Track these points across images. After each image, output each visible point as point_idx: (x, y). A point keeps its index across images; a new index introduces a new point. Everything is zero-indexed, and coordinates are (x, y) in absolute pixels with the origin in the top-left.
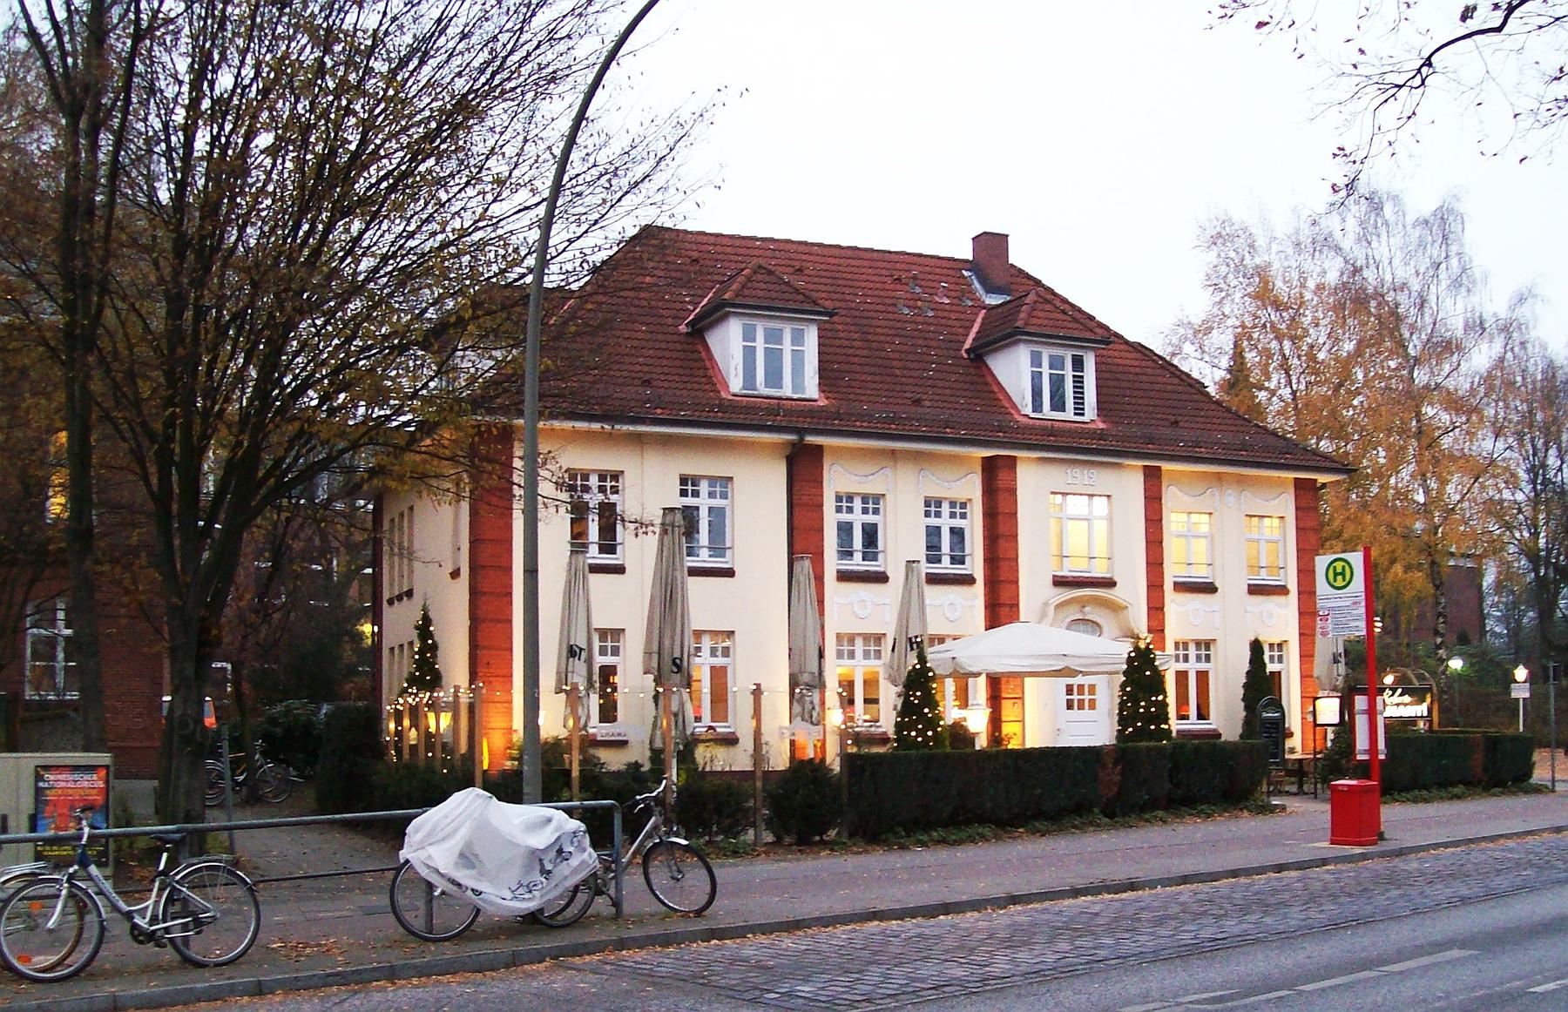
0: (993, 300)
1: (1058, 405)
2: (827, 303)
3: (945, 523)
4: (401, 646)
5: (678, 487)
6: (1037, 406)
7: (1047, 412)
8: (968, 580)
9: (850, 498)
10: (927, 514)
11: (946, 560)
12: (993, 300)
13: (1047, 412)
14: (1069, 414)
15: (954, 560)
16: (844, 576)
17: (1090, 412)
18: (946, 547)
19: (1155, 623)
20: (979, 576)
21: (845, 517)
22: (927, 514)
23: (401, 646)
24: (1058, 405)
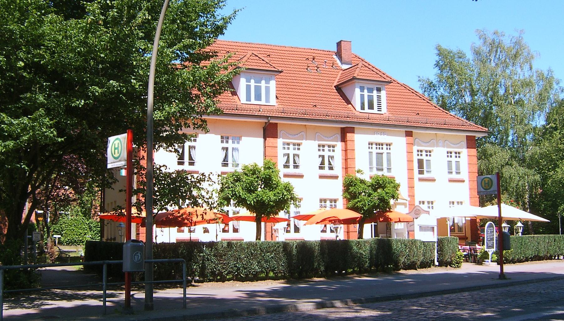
0: (345, 67)
1: (258, 97)
2: (278, 68)
3: (326, 154)
4: (112, 203)
5: (220, 140)
6: (248, 99)
7: (253, 101)
8: (336, 177)
9: (451, 153)
10: (319, 150)
11: (454, 173)
12: (345, 67)
13: (367, 110)
14: (263, 102)
15: (378, 169)
16: (420, 180)
17: (384, 110)
18: (454, 170)
19: (411, 194)
20: (466, 179)
21: (420, 157)
22: (319, 150)
23: (112, 203)
24: (258, 97)
